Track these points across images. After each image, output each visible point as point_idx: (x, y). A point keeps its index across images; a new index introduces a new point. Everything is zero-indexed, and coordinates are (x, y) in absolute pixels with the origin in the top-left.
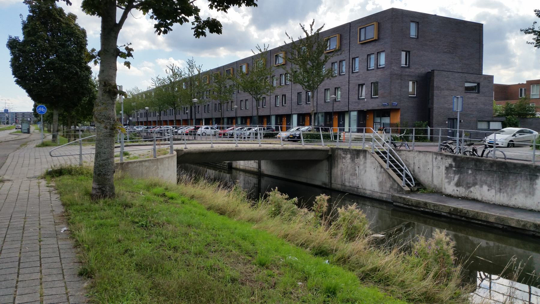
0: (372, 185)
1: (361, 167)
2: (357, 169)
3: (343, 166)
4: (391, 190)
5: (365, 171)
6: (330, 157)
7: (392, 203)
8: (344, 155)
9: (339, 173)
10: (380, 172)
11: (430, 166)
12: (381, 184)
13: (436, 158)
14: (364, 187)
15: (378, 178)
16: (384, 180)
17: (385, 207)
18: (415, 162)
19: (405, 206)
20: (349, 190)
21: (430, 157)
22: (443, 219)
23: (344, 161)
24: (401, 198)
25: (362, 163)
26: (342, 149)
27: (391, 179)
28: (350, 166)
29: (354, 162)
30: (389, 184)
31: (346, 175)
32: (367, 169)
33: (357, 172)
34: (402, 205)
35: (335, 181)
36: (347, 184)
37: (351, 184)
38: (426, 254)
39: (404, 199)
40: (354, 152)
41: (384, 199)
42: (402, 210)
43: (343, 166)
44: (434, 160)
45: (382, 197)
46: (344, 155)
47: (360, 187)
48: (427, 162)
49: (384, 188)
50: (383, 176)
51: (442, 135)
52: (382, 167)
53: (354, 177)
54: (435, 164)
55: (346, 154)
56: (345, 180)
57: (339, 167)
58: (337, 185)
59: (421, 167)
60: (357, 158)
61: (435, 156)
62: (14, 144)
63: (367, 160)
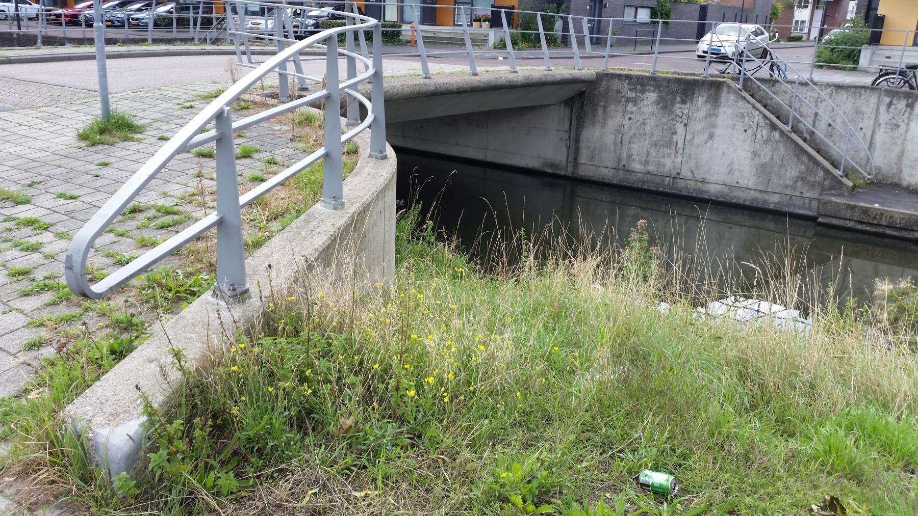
0: (730, 172)
1: (697, 126)
2: (680, 129)
3: (627, 123)
4: (799, 184)
5: (711, 136)
6: (581, 100)
7: (813, 219)
8: (631, 95)
9: (610, 139)
10: (767, 141)
11: (868, 124)
12: (763, 170)
13: (890, 104)
14: (699, 176)
15: (755, 154)
16: (777, 159)
17: (771, 225)
18: (820, 112)
19: (859, 227)
20: (643, 182)
21: (869, 103)
22: (888, 241)
23: (631, 107)
24: (853, 208)
25: (701, 114)
26: (628, 77)
27: (805, 159)
28: (652, 122)
29: (671, 112)
30: (792, 170)
31: (635, 146)
32: (718, 131)
33: (679, 138)
34: (850, 224)
35: (592, 158)
36: (637, 166)
37: (650, 168)
38: (434, 260)
39: (866, 211)
40: (675, 87)
41: (772, 206)
42: (847, 235)
43: (627, 123)
44: (883, 109)
45: (765, 202)
46: (631, 95)
47: (686, 173)
48: (858, 112)
49: (775, 179)
50: (775, 150)
51: (204, 13)
52: (774, 127)
53: (667, 151)
54: (884, 117)
55: (643, 92)
56: (629, 157)
57: (612, 124)
58: (586, 170)
59: (838, 125)
60: (683, 102)
61: (887, 100)
62: (681, 242)
63: (722, 110)
